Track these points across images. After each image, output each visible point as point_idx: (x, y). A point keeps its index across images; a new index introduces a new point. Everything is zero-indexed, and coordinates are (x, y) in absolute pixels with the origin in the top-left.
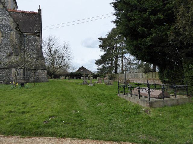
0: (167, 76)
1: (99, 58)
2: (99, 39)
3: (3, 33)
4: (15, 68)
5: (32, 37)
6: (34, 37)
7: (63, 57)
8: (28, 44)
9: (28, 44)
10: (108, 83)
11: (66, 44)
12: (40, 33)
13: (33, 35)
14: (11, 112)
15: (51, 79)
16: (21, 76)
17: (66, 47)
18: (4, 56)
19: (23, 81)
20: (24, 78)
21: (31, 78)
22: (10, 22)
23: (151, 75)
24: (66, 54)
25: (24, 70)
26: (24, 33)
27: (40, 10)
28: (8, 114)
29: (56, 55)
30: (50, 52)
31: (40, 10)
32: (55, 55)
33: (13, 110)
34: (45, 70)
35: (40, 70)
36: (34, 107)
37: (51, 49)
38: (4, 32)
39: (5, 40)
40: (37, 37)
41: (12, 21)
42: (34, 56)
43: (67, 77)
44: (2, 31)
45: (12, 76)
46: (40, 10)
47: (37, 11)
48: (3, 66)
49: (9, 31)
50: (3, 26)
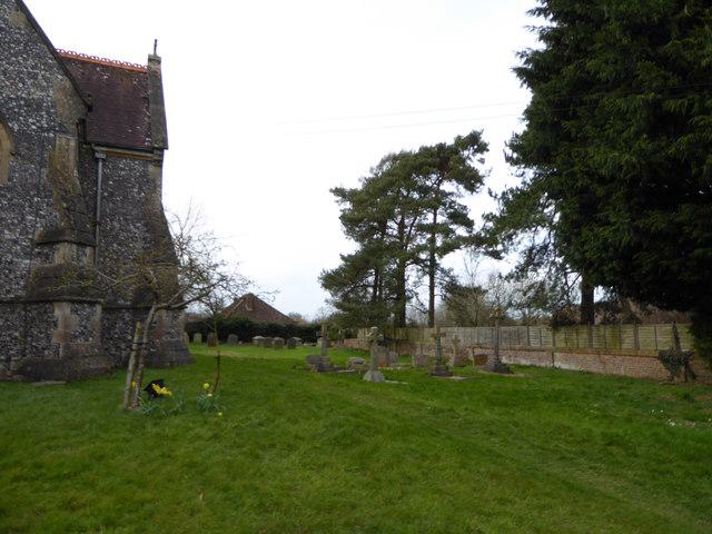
0: (112, 298)
1: (335, 264)
2: (331, 191)
3: (19, 138)
4: (73, 302)
8: (112, 194)
9: (112, 194)
10: (437, 370)
13: (134, 158)
18: (15, 242)
21: (118, 348)
23: (585, 336)
26: (96, 148)
31: (154, 60)
38: (22, 133)
39: (25, 171)
41: (63, 89)
44: (16, 128)
46: (154, 60)
47: (144, 62)
48: (8, 292)
49: (48, 130)
50: (20, 107)
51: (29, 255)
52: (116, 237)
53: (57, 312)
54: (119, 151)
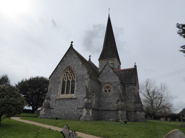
5: (131, 87)
6: (132, 86)
7: (162, 98)
8: (129, 92)
11: (163, 85)
12: (137, 84)
14: (120, 134)
15: (152, 121)
16: (125, 117)
17: (164, 88)
19: (126, 120)
20: (127, 118)
22: (116, 79)
24: (165, 95)
25: (127, 112)
27: (135, 66)
28: (118, 135)
29: (155, 97)
30: (149, 94)
32: (153, 96)
33: (121, 134)
34: (142, 112)
35: (138, 112)
36: (130, 134)
37: (150, 91)
40: (134, 86)
42: (133, 101)
43: (168, 119)
45: (119, 116)
47: (134, 67)
51: (116, 103)
52: (130, 99)
53: (119, 112)
54: (93, 78)
